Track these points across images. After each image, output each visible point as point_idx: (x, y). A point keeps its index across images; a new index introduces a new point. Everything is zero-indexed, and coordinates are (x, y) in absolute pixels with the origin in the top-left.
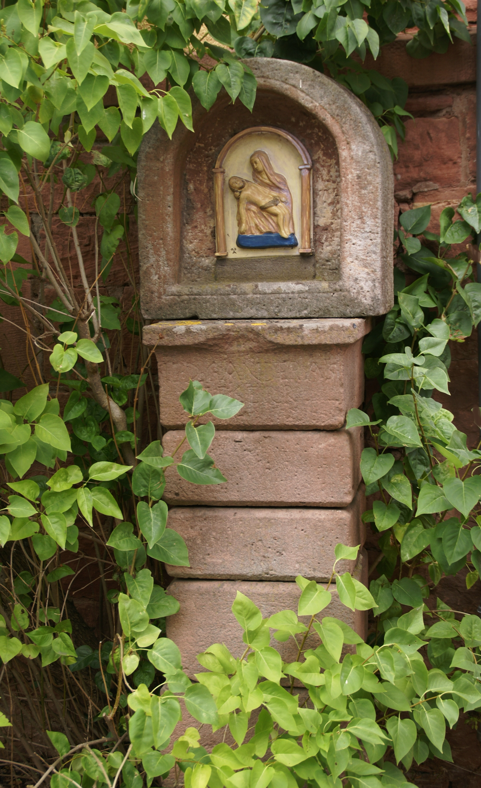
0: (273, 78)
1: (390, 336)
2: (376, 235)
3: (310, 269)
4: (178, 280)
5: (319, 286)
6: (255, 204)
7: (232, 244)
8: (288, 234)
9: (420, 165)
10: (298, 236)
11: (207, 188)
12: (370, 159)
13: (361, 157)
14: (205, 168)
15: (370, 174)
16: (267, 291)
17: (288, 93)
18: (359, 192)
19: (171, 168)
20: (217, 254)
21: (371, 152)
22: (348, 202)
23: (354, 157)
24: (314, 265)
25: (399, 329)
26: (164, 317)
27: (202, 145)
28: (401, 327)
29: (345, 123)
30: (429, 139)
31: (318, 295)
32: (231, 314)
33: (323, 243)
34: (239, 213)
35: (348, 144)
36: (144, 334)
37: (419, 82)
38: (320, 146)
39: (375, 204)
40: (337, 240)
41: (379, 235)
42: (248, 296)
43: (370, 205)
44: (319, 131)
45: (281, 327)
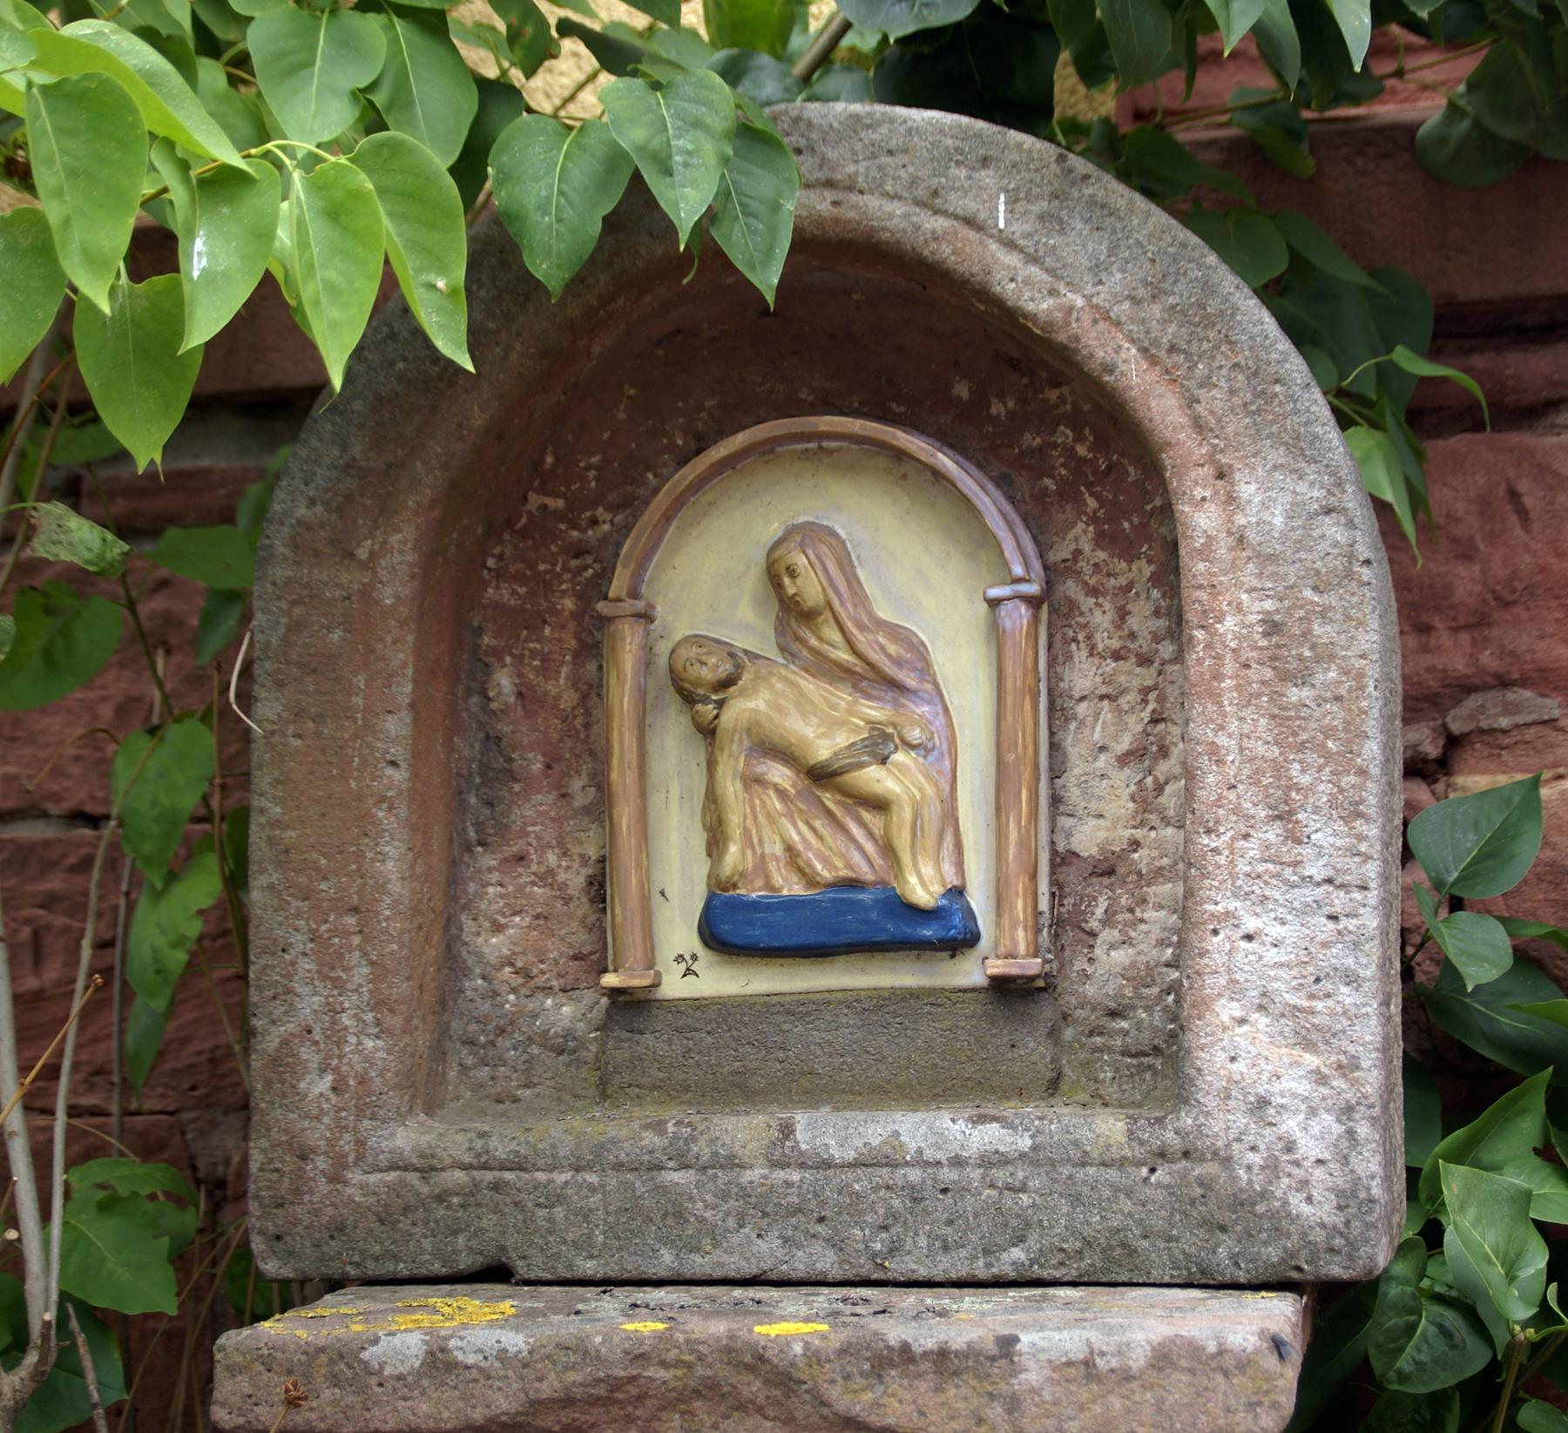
0: (877, 188)
1: (1404, 1363)
2: (1357, 895)
3: (1034, 1048)
4: (425, 1090)
5: (1083, 1134)
6: (784, 753)
7: (678, 932)
8: (937, 889)
9: (1477, 623)
10: (979, 900)
11: (575, 686)
12: (1324, 546)
13: (1283, 534)
14: (569, 604)
15: (1324, 613)
16: (836, 1153)
17: (945, 252)
18: (1275, 696)
19: (406, 592)
20: (610, 980)
21: (1329, 511)
22: (1222, 740)
23: (1251, 534)
24: (1054, 1034)
25: (1442, 1328)
26: (352, 1271)
27: (559, 504)
28: (1451, 1318)
29: (1206, 383)
30: (1514, 518)
31: (1080, 1174)
32: (666, 1261)
33: (1093, 934)
34: (712, 798)
35: (1221, 476)
36: (219, 1371)
37: (1471, 286)
38: (1079, 502)
39: (1350, 751)
40: (1157, 919)
41: (1373, 896)
42: (748, 1176)
43: (1328, 756)
44: (1079, 439)
45: (905, 1348)
